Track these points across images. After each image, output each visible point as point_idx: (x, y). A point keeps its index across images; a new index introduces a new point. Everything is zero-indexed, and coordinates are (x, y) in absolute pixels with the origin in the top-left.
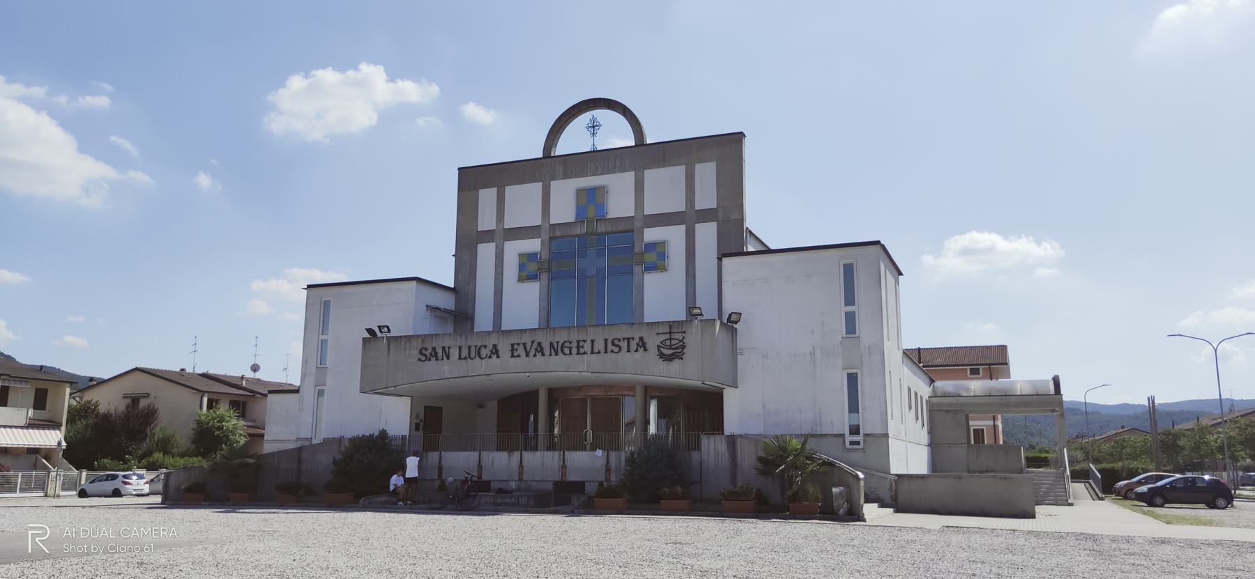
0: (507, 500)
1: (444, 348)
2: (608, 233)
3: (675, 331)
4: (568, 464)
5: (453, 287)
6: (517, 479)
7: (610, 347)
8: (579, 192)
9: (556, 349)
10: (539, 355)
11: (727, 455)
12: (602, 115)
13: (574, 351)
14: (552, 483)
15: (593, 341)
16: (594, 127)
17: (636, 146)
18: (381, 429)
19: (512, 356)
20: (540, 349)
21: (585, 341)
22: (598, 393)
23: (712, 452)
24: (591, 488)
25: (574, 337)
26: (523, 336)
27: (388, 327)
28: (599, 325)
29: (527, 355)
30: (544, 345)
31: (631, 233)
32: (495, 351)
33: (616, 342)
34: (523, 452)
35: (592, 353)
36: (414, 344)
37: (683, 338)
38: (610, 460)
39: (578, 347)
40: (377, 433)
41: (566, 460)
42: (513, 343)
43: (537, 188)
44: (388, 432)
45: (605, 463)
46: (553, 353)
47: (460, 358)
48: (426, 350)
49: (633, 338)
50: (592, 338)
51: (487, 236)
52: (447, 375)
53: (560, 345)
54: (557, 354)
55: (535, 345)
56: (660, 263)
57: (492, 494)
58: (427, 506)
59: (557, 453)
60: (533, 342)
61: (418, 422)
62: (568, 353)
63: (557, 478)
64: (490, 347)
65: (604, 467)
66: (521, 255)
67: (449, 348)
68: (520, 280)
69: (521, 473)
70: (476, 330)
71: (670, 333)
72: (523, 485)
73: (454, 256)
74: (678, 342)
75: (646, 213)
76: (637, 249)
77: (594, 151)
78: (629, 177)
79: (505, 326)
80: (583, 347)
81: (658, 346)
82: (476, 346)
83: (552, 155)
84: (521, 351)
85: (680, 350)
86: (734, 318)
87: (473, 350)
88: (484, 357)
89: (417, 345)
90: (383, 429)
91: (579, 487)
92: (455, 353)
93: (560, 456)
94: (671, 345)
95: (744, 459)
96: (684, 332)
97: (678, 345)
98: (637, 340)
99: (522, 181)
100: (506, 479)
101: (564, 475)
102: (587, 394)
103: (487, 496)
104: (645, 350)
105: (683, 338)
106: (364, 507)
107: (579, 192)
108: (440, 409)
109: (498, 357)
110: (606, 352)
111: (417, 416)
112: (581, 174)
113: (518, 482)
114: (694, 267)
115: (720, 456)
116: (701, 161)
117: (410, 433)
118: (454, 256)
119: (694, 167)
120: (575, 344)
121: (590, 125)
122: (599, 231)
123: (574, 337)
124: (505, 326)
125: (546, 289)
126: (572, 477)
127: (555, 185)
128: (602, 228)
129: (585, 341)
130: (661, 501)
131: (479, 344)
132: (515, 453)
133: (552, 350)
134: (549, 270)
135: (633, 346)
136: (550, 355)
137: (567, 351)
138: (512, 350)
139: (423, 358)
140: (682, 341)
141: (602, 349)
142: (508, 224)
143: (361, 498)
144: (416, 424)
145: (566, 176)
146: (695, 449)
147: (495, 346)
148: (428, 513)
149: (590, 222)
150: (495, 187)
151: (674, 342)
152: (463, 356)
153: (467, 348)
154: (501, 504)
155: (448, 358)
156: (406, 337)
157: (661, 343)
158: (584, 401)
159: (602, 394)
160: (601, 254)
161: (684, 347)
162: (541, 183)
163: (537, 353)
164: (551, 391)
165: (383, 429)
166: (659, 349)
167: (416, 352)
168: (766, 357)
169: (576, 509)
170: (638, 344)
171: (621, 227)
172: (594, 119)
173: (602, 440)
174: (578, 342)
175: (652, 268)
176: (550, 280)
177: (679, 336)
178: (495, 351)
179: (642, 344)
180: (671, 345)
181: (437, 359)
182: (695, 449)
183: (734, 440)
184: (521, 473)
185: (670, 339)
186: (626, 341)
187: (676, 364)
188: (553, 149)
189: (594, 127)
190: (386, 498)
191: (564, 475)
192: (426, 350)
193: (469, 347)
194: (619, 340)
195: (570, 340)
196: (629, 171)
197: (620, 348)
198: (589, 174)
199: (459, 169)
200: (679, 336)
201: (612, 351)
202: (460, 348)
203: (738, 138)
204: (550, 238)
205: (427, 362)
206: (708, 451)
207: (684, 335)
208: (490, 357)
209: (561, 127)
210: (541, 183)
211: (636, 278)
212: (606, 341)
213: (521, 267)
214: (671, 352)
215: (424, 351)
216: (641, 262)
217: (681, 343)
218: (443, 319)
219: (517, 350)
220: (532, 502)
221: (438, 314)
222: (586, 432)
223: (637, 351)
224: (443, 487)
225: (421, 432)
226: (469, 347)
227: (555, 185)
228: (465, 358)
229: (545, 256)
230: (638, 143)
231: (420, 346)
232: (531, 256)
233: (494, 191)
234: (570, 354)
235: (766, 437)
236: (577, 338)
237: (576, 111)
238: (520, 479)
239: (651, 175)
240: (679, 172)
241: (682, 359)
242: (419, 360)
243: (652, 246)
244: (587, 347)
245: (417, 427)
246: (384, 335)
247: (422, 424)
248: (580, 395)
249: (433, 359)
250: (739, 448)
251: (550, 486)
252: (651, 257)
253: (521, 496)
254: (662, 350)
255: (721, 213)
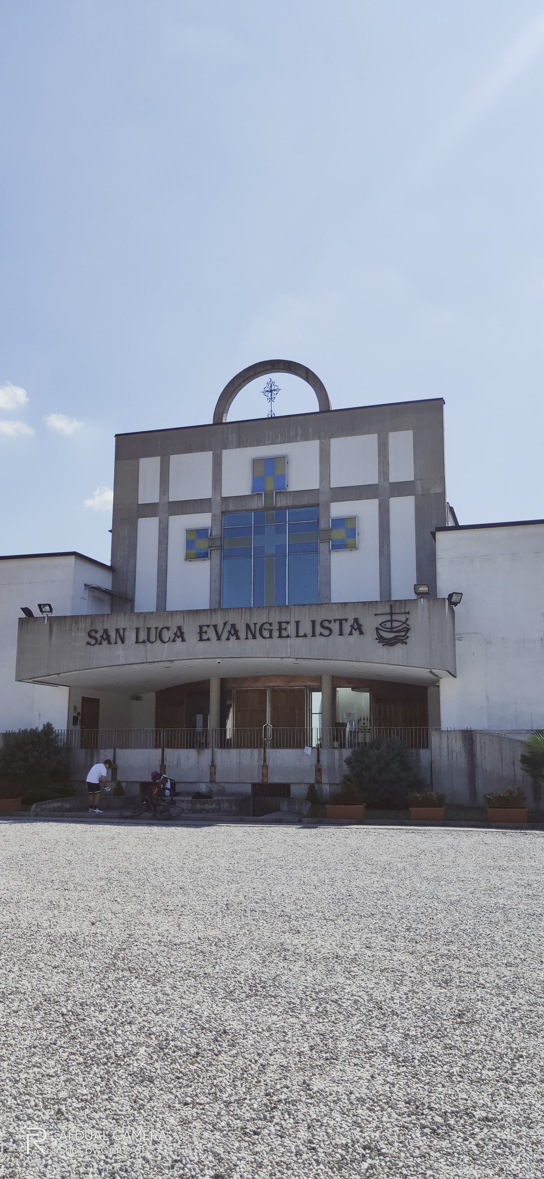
0: (207, 806)
1: (117, 631)
2: (289, 508)
3: (397, 611)
4: (270, 763)
5: (109, 565)
6: (208, 781)
7: (319, 629)
8: (256, 462)
9: (252, 632)
10: (233, 638)
11: (463, 752)
12: (280, 378)
13: (276, 634)
14: (250, 786)
15: (297, 623)
16: (271, 391)
17: (320, 412)
18: (46, 723)
19: (201, 640)
20: (234, 632)
21: (288, 623)
22: (279, 684)
23: (445, 747)
24: (298, 791)
25: (275, 618)
26: (214, 615)
27: (50, 606)
28: (304, 605)
29: (219, 638)
30: (238, 627)
31: (315, 508)
32: (180, 634)
33: (326, 624)
34: (216, 750)
35: (297, 636)
36: (82, 625)
37: (407, 619)
38: (321, 759)
39: (280, 630)
40: (40, 728)
41: (267, 759)
42: (201, 624)
43: (206, 457)
44: (53, 726)
45: (315, 762)
46: (250, 636)
47: (137, 642)
48: (96, 632)
49: (346, 620)
50: (297, 620)
51: (150, 510)
52: (122, 661)
53: (258, 627)
54: (254, 637)
55: (228, 627)
56: (349, 541)
57: (190, 798)
58: (117, 813)
59: (256, 751)
60: (225, 624)
61: (76, 715)
62: (268, 636)
63: (257, 780)
64: (175, 629)
65: (314, 769)
66: (189, 532)
67: (124, 629)
68: (189, 558)
69: (213, 774)
70: (137, 610)
71: (391, 614)
72: (215, 789)
73: (110, 531)
74: (401, 624)
75: (333, 485)
76: (323, 525)
77: (272, 418)
78: (313, 447)
79: (171, 605)
80: (285, 629)
81: (377, 629)
82: (156, 628)
83: (224, 421)
84: (211, 634)
85: (403, 634)
86: (454, 599)
87: (153, 632)
88: (167, 640)
89: (85, 626)
90: (48, 723)
91: (283, 789)
92: (131, 636)
93: (259, 755)
94: (392, 628)
95: (485, 758)
96: (408, 613)
97: (401, 628)
98: (351, 622)
99: (190, 449)
100: (195, 781)
101: (265, 775)
102: (267, 685)
103: (183, 801)
104: (361, 633)
105: (407, 619)
106: (36, 815)
107: (256, 462)
108: (97, 701)
109: (183, 640)
110: (314, 635)
111: (75, 708)
112: (258, 442)
113: (208, 785)
114: (388, 546)
115: (454, 755)
116: (395, 430)
117: (68, 728)
118: (110, 531)
119: (388, 436)
120: (275, 627)
121: (267, 389)
122: (279, 505)
123: (275, 618)
124: (171, 605)
125: (218, 568)
126: (274, 779)
127: (228, 455)
128: (281, 502)
129: (288, 623)
130: (410, 808)
131: (161, 627)
132: (206, 750)
133: (249, 633)
134: (221, 547)
135: (347, 628)
136: (247, 638)
137: (266, 634)
138: (201, 633)
139: (93, 642)
140: (405, 623)
141: (309, 632)
142: (173, 496)
143: (32, 804)
144: (74, 717)
145: (241, 444)
146: (412, 747)
147: (179, 628)
148: (118, 824)
149: (268, 495)
150: (158, 455)
151: (395, 624)
152: (141, 640)
153: (146, 631)
154: (200, 811)
155: (123, 642)
156: (72, 617)
157: (380, 625)
158: (263, 692)
159: (283, 684)
160: (280, 530)
161: (407, 630)
162: (212, 452)
163: (231, 637)
164: (223, 682)
165: (48, 723)
166: (377, 632)
167: (83, 636)
168: (488, 643)
169: (304, 817)
170: (352, 627)
171: (305, 501)
172: (271, 383)
173: (412, 737)
174: (280, 623)
175: (340, 546)
176: (223, 558)
177: (403, 618)
178: (180, 634)
179: (358, 627)
180: (392, 628)
181: (109, 643)
182: (412, 747)
183: (472, 736)
184: (213, 774)
185: (392, 621)
186: (338, 623)
187: (398, 650)
188: (224, 415)
189: (271, 391)
190: (59, 804)
191: (265, 775)
192: (96, 632)
193: (149, 629)
194: (330, 622)
195: (270, 621)
196: (313, 439)
197: (331, 631)
198: (267, 443)
199: (116, 436)
200: (403, 618)
201: (321, 634)
202: (138, 630)
203: (440, 401)
204: (222, 512)
205: (97, 646)
206: (440, 748)
207: (408, 616)
208: (174, 641)
209: (234, 391)
210: (212, 452)
211: (322, 558)
212: (313, 622)
213: (189, 544)
214: (392, 635)
215: (93, 634)
216: (327, 540)
217: (404, 625)
218: (99, 600)
219: (206, 632)
220: (234, 808)
221: (96, 594)
222: (265, 727)
223: (351, 634)
224: (119, 790)
225: (78, 728)
226: (149, 629)
227: (228, 455)
228: (144, 642)
229: (216, 532)
230: (323, 409)
231: (89, 628)
232: (201, 533)
233: (157, 460)
234: (271, 637)
235: (519, 732)
236: (278, 620)
237: (252, 373)
238: (212, 781)
239: (337, 444)
240: (371, 440)
241: (406, 643)
242: (88, 643)
243: (339, 522)
244: (291, 629)
245: (75, 721)
246: (45, 615)
247: (80, 717)
248: (259, 686)
249: (105, 643)
250: (478, 745)
251: (248, 789)
252: (339, 534)
253: (223, 800)
254: (382, 633)
255: (419, 488)
